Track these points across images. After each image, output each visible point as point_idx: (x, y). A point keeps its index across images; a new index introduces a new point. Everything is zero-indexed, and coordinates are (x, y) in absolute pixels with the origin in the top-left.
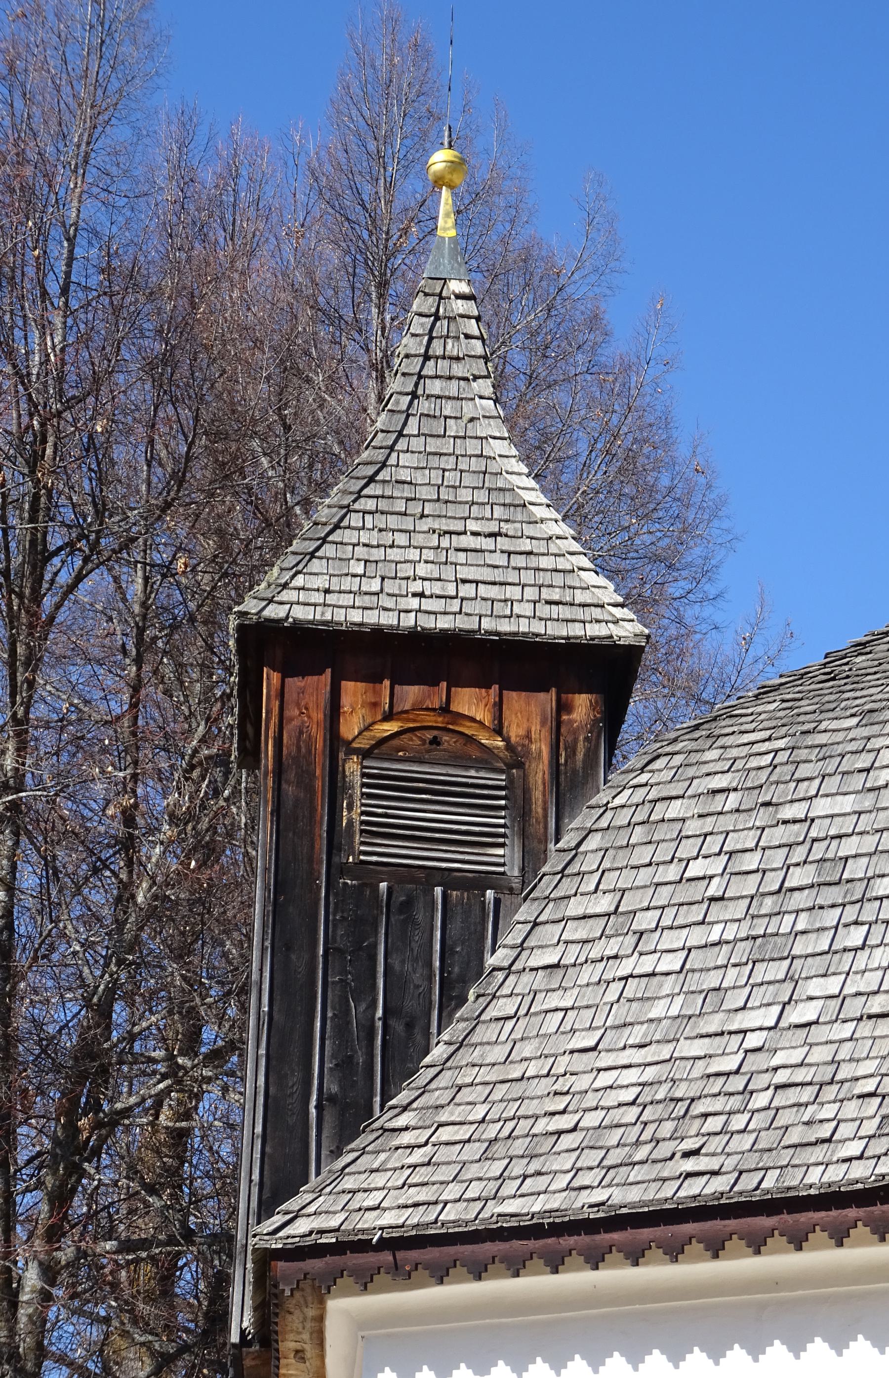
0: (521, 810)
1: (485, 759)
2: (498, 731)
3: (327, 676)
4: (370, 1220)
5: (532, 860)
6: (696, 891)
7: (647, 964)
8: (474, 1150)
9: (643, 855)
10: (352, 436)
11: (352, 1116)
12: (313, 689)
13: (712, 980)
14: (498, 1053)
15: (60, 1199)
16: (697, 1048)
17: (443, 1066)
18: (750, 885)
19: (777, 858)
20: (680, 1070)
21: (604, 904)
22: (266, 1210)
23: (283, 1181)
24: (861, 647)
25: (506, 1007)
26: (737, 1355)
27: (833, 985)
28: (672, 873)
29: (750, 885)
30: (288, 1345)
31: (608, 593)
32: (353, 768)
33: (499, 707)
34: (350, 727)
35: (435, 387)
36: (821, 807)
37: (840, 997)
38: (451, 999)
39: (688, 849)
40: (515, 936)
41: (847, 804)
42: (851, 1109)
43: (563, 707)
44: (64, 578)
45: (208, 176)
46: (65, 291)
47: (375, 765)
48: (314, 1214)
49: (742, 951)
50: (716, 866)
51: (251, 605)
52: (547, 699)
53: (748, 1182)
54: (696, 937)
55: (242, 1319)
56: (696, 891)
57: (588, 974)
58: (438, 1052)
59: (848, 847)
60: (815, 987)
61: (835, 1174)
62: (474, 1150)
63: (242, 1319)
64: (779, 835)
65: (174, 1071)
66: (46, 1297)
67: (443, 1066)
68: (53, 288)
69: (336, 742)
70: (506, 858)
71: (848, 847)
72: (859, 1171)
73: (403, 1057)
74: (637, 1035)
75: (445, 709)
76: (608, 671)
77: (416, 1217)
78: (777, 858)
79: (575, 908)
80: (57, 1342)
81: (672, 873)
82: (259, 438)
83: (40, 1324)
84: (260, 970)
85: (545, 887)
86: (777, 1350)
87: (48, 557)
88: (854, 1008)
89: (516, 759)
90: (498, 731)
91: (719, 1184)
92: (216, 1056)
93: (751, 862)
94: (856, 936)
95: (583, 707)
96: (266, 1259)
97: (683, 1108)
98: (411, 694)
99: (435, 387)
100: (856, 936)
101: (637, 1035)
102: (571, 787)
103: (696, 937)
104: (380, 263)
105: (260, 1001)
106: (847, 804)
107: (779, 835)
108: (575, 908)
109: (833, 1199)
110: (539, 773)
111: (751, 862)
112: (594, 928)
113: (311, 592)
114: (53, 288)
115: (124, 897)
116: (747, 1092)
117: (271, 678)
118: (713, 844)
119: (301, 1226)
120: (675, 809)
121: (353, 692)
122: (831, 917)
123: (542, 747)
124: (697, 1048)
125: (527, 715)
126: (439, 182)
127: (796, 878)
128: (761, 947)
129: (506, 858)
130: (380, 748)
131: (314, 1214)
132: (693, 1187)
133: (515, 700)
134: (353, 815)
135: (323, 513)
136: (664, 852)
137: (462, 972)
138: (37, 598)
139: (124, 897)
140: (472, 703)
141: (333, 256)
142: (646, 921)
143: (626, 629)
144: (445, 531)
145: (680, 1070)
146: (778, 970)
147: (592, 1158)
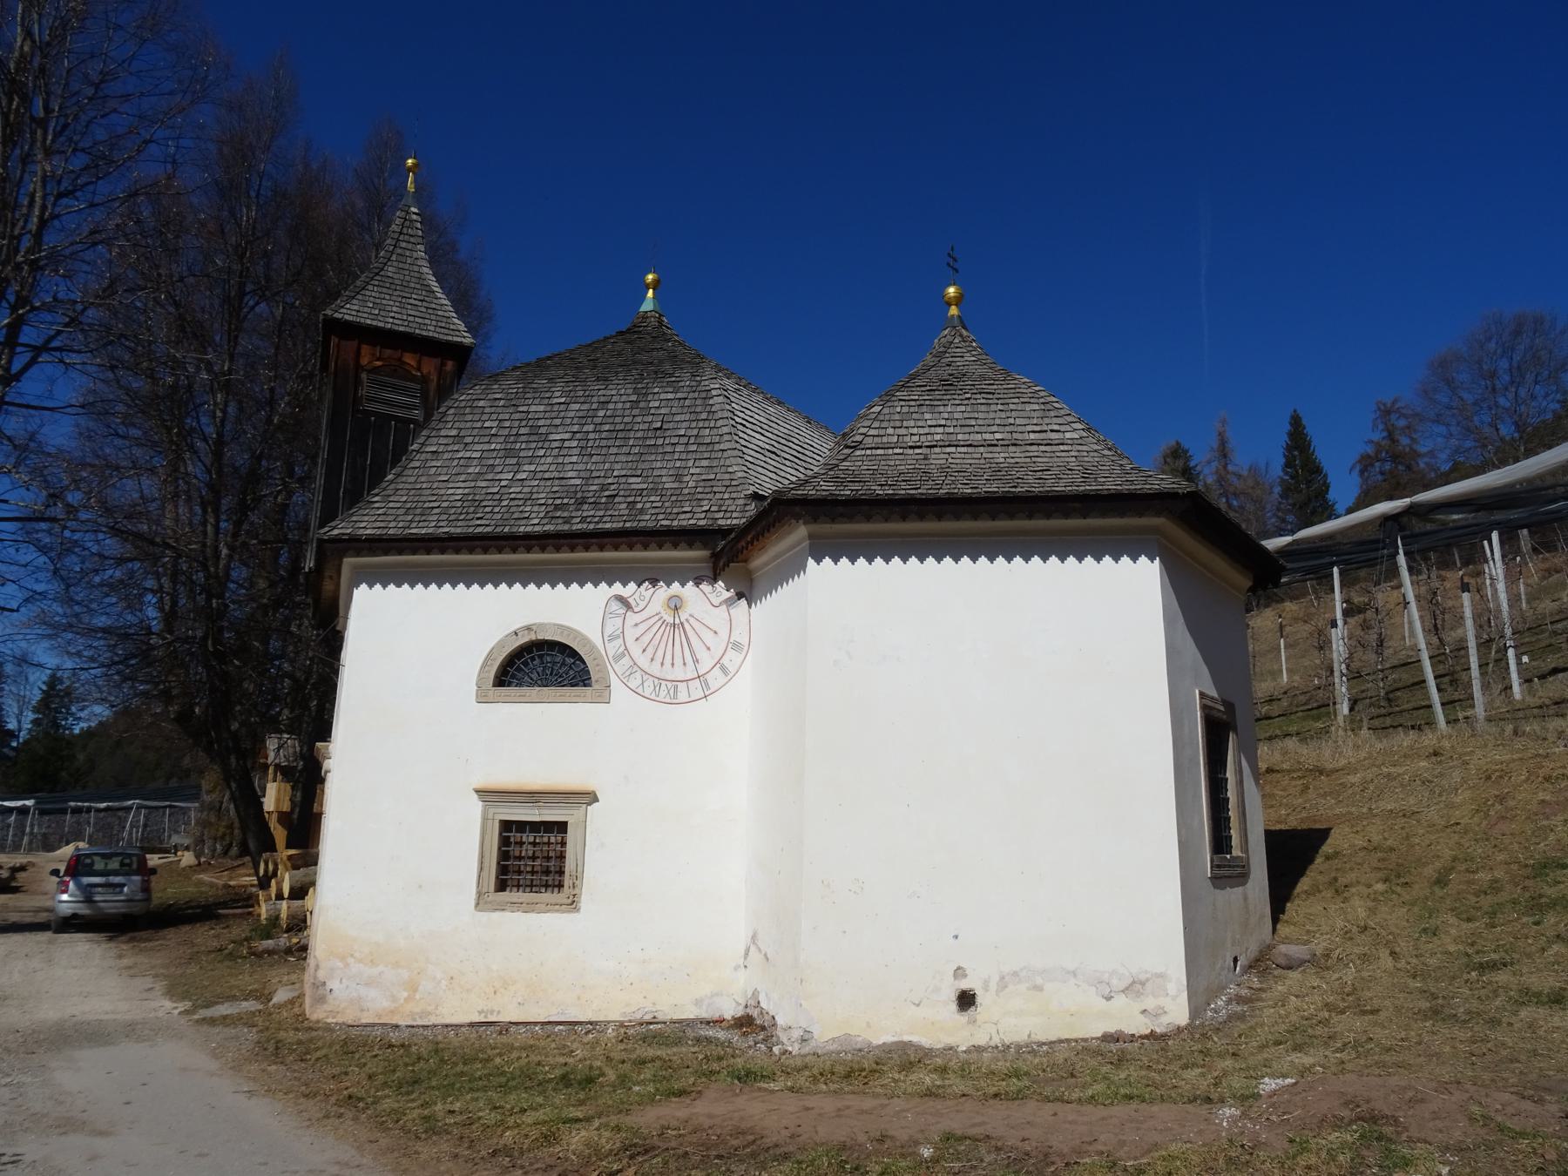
0: (425, 397)
1: (413, 379)
2: (419, 369)
3: (355, 343)
4: (361, 532)
5: (428, 417)
6: (487, 432)
7: (468, 454)
8: (402, 511)
9: (469, 417)
10: (364, 267)
11: (356, 497)
12: (351, 345)
13: (491, 462)
14: (412, 479)
15: (238, 524)
16: (484, 484)
17: (392, 482)
18: (506, 432)
19: (516, 424)
20: (477, 491)
21: (454, 433)
22: (322, 526)
23: (328, 516)
24: (549, 358)
25: (417, 464)
26: (490, 587)
27: (532, 468)
28: (479, 425)
29: (506, 432)
30: (327, 574)
31: (462, 327)
32: (364, 376)
33: (419, 362)
34: (364, 361)
35: (404, 245)
36: (533, 408)
37: (535, 472)
38: (396, 461)
39: (485, 417)
40: (421, 440)
41: (542, 408)
42: (536, 508)
43: (443, 364)
44: (251, 303)
45: (314, 166)
46: (257, 196)
47: (372, 376)
48: (339, 529)
49: (501, 454)
50: (495, 424)
51: (329, 312)
52: (437, 361)
53: (499, 529)
54: (486, 447)
55: (309, 563)
56: (487, 432)
57: (446, 456)
58: (390, 477)
59: (541, 423)
60: (526, 468)
61: (529, 529)
62: (402, 511)
63: (309, 563)
64: (517, 416)
65: (284, 484)
66: (230, 557)
67: (392, 482)
68: (253, 194)
69: (358, 367)
70: (417, 414)
71: (541, 423)
72: (537, 528)
73: (377, 478)
74: (463, 478)
75: (400, 359)
76: (460, 354)
77: (379, 532)
78: (516, 424)
79: (443, 433)
80: (234, 574)
81: (479, 425)
82: (331, 250)
83: (228, 568)
84: (324, 441)
85: (433, 424)
86: (575, 586)
87: (245, 294)
88: (539, 476)
89: (424, 380)
90: (419, 369)
91: (489, 529)
92: (301, 480)
93: (507, 424)
94: (541, 452)
95: (450, 365)
96: (321, 542)
97: (478, 504)
98: (388, 352)
99: (404, 245)
100: (541, 452)
101: (463, 478)
102: (444, 392)
103: (486, 447)
104: (380, 204)
105: (323, 455)
106: (542, 408)
107: (517, 416)
108: (443, 433)
109: (527, 537)
110: (433, 386)
111: (507, 424)
112: (450, 440)
113: (350, 311)
114: (253, 194)
115: (269, 421)
116: (500, 500)
117: (334, 340)
118: (494, 417)
119: (336, 532)
120: (481, 403)
121: (365, 349)
122: (533, 445)
123: (434, 378)
124: (484, 484)
125: (429, 366)
126: (410, 170)
127: (522, 431)
128: (509, 452)
129: (417, 414)
130: (375, 370)
131: (339, 529)
132: (480, 530)
133: (425, 359)
134: (363, 392)
135: (358, 283)
136: (476, 417)
137: (400, 452)
138: (241, 309)
139: (269, 421)
140: (410, 359)
141: (360, 204)
142: (468, 440)
143: (468, 340)
144: (404, 296)
145: (477, 491)
146: (514, 461)
147: (444, 517)
